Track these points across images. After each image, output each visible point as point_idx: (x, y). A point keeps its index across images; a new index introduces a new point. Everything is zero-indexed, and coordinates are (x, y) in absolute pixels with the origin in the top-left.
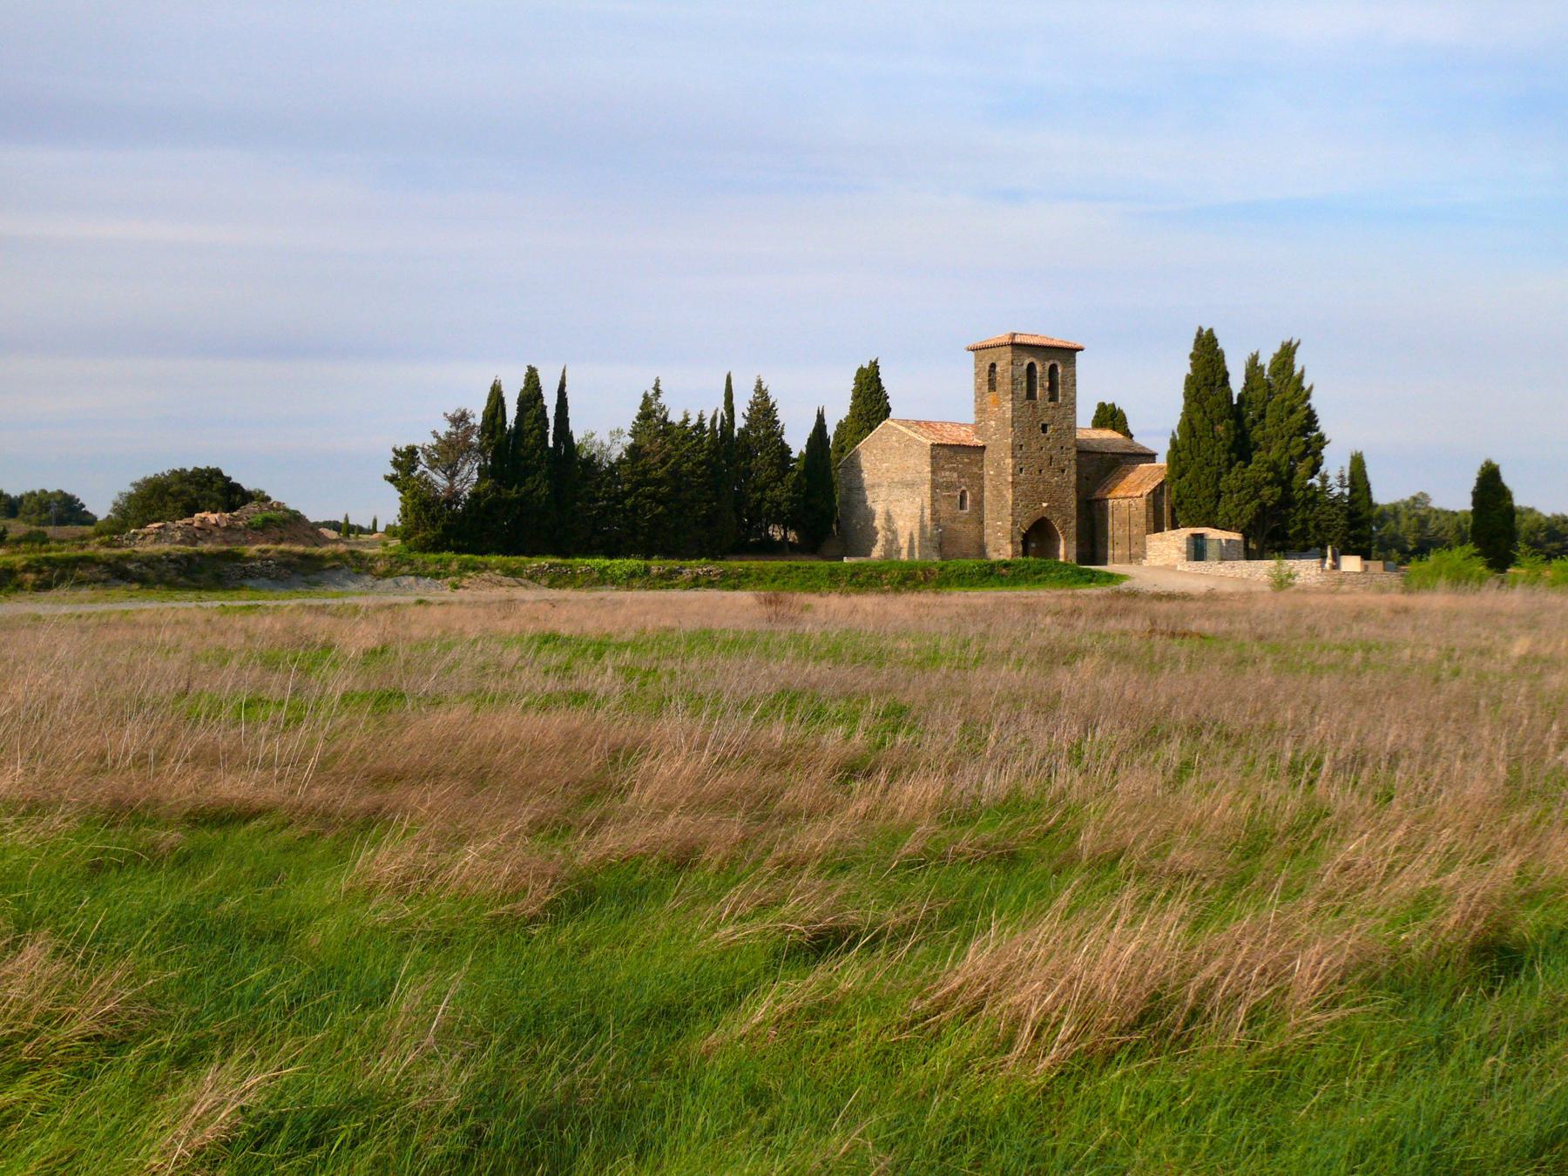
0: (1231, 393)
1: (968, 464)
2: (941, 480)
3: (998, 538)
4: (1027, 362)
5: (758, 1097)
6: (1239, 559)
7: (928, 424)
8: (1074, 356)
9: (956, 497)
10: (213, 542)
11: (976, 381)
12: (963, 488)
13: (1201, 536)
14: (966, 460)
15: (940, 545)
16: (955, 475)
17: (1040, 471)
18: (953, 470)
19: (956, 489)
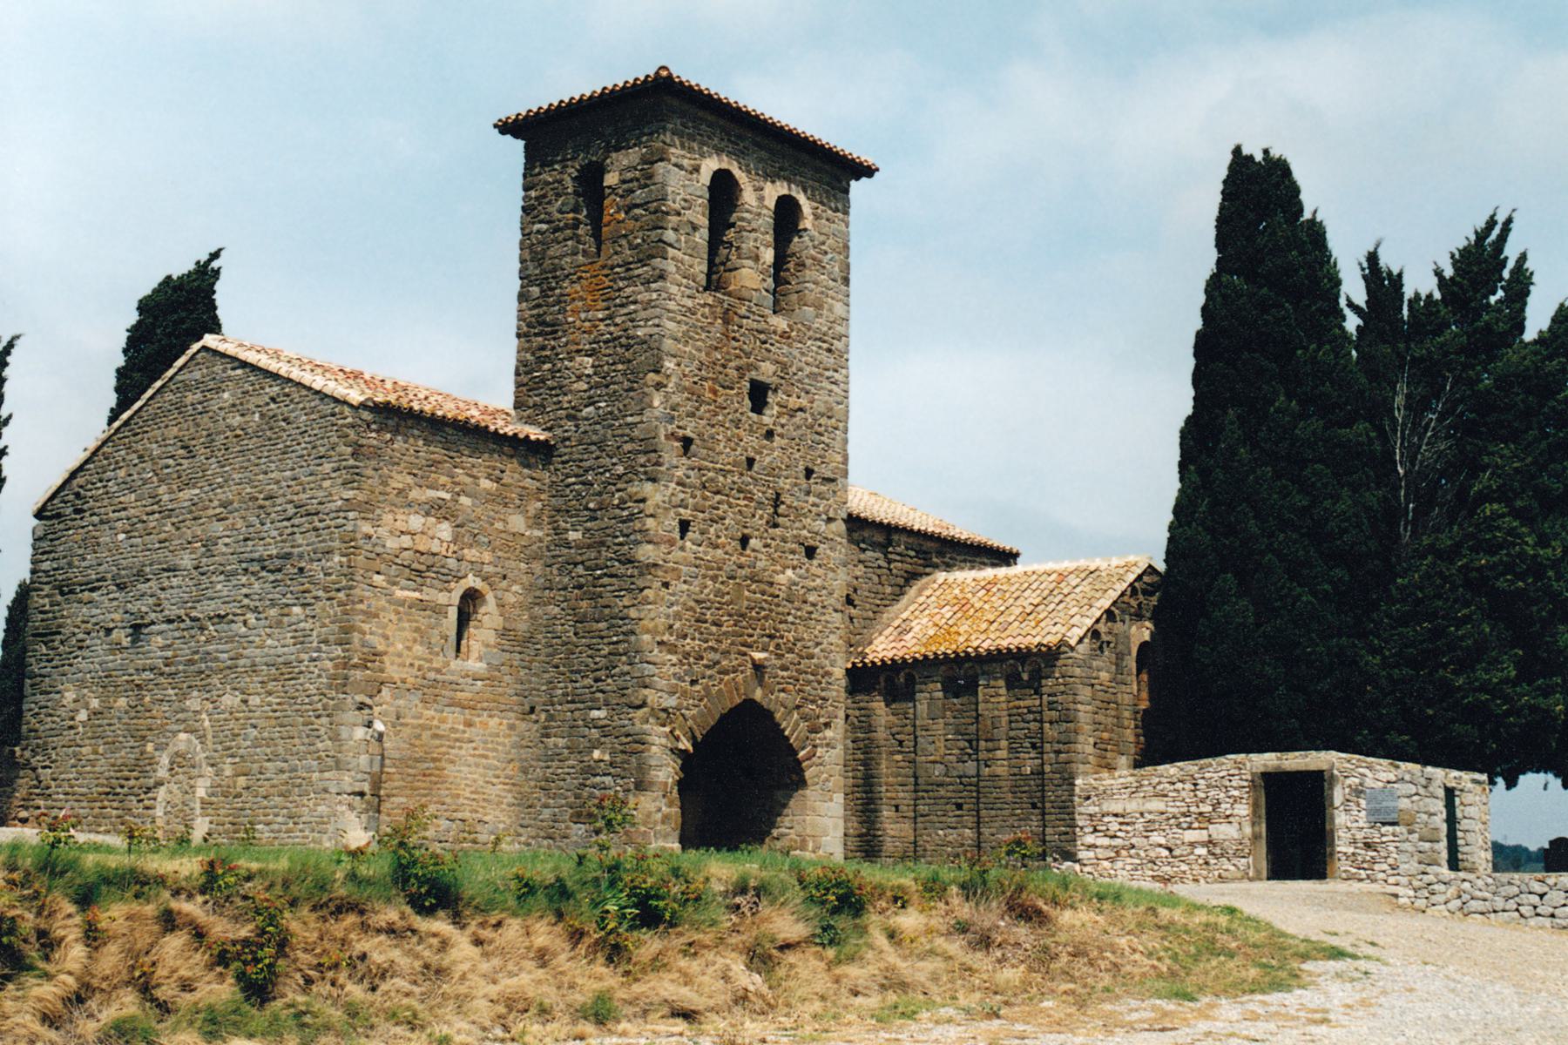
0: (1402, 295)
1: (491, 498)
2: (392, 544)
3: (590, 771)
4: (710, 165)
5: (213, 1021)
6: (1258, 878)
7: (357, 376)
8: (846, 191)
9: (439, 610)
10: (765, 981)
11: (526, 235)
12: (472, 581)
13: (1317, 782)
14: (486, 484)
15: (377, 784)
16: (445, 530)
17: (744, 541)
18: (436, 510)
19: (448, 577)
